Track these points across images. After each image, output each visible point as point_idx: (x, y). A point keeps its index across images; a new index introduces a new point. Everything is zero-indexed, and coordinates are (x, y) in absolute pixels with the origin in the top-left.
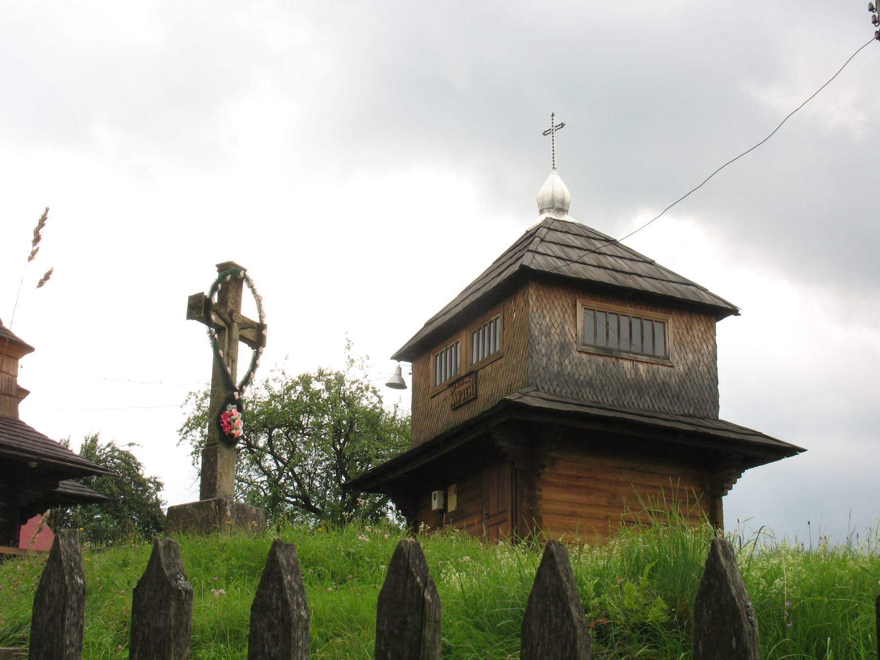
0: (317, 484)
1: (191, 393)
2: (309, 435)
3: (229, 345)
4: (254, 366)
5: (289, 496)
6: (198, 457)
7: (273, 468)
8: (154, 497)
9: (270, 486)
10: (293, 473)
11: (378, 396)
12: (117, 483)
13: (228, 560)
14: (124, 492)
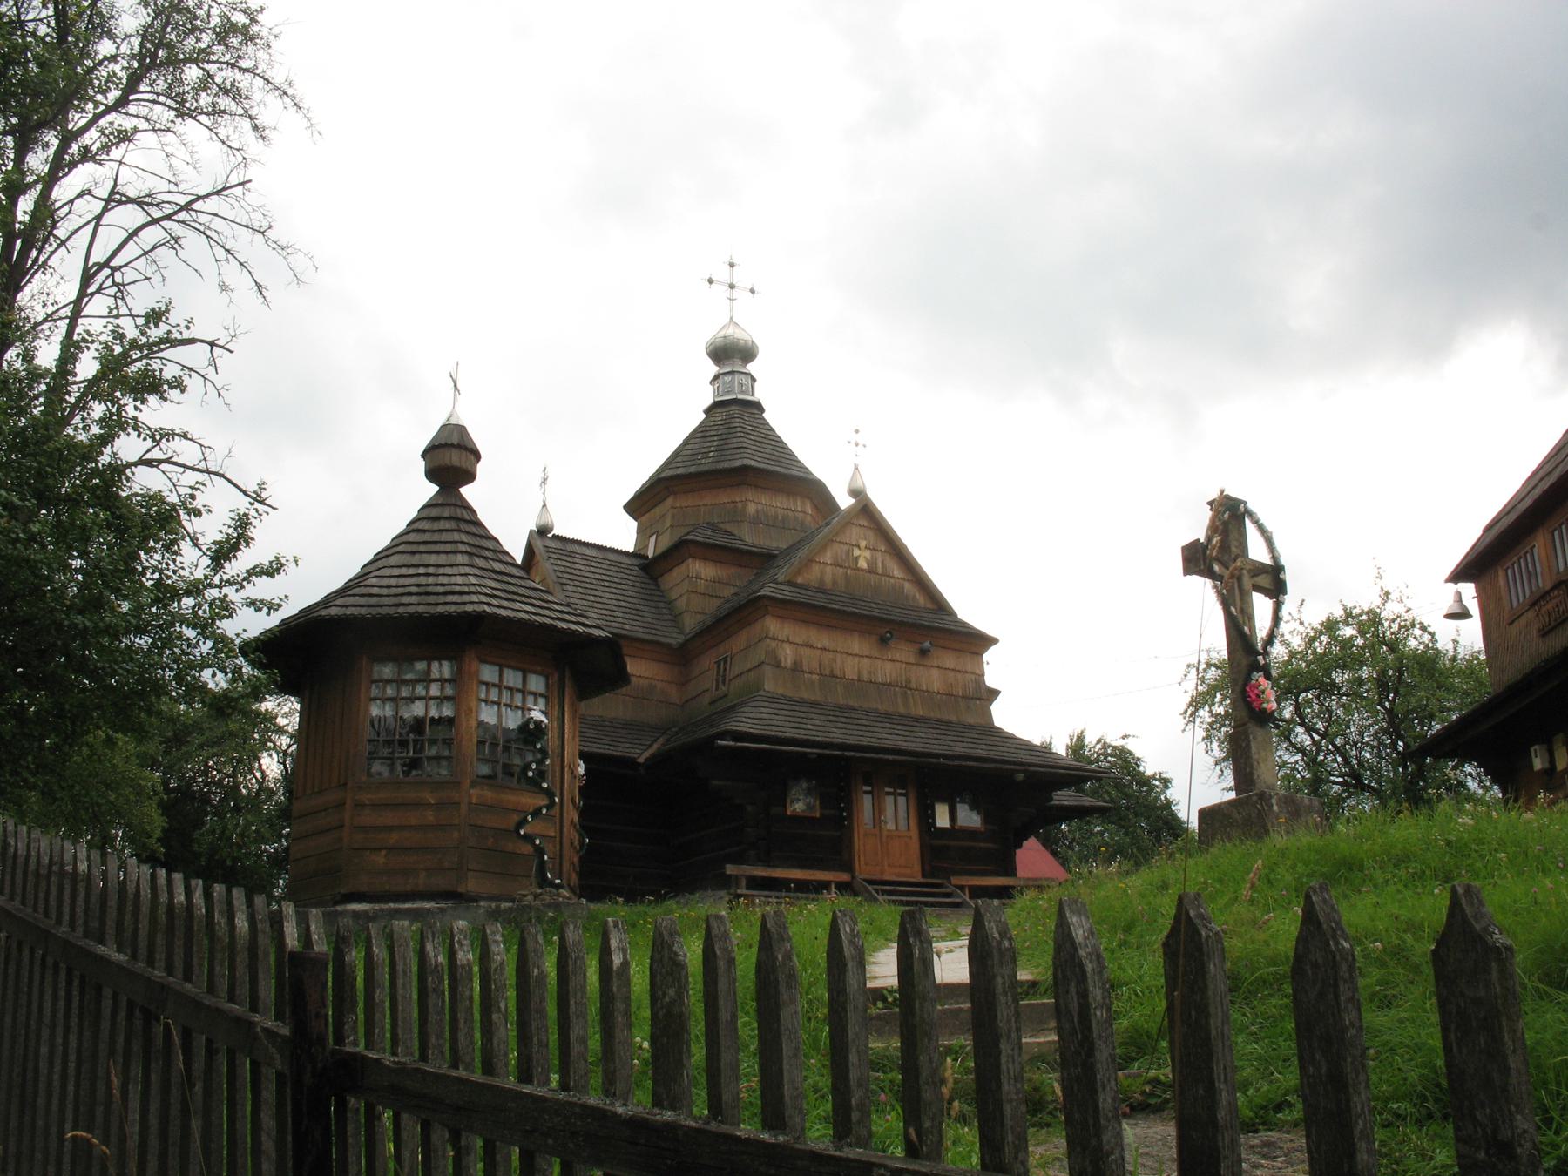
0: (1368, 756)
1: (1188, 666)
2: (1347, 695)
3: (1241, 599)
4: (1276, 620)
5: (1333, 775)
6: (1211, 742)
7: (1308, 743)
8: (1162, 797)
9: (1307, 767)
10: (1334, 745)
11: (1430, 633)
12: (1115, 787)
13: (1293, 867)
14: (1127, 796)
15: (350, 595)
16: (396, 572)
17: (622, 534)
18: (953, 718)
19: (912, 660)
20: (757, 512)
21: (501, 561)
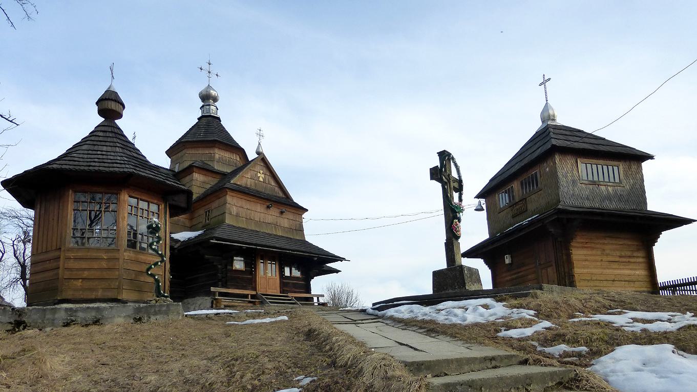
3: (450, 191)
15: (63, 160)
16: (86, 152)
17: (164, 162)
18: (292, 237)
19: (278, 215)
20: (219, 158)
21: (137, 153)
